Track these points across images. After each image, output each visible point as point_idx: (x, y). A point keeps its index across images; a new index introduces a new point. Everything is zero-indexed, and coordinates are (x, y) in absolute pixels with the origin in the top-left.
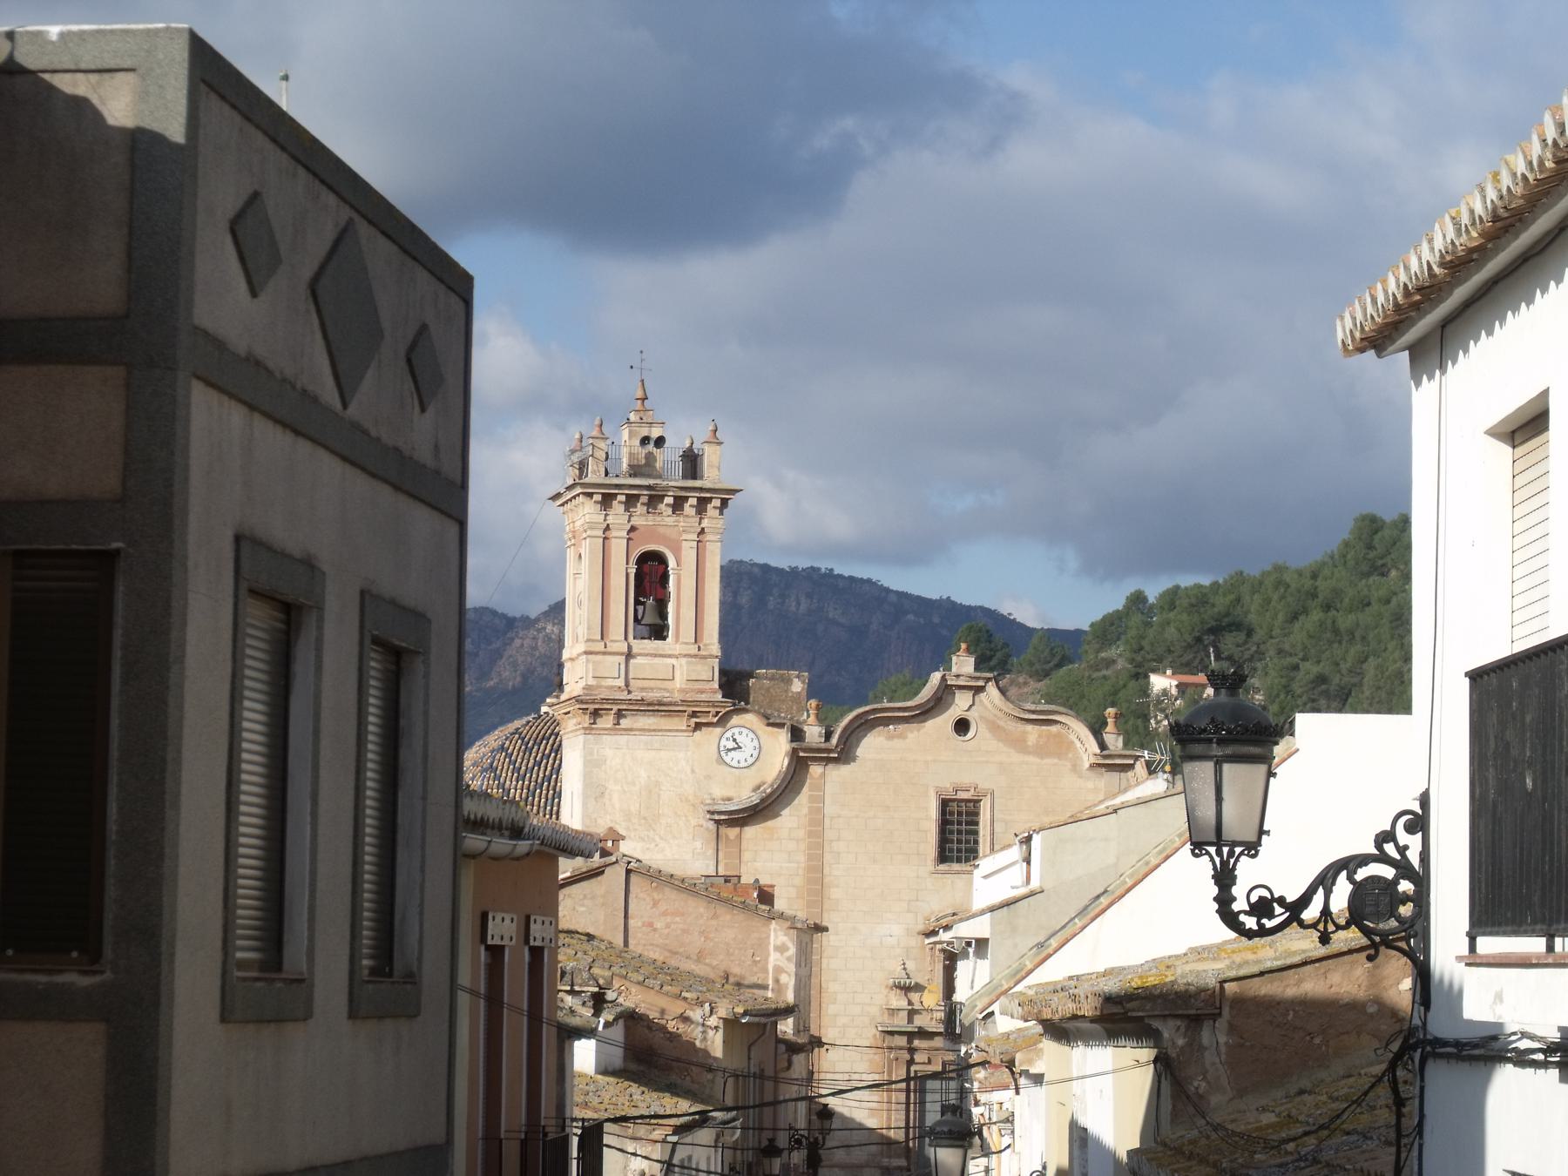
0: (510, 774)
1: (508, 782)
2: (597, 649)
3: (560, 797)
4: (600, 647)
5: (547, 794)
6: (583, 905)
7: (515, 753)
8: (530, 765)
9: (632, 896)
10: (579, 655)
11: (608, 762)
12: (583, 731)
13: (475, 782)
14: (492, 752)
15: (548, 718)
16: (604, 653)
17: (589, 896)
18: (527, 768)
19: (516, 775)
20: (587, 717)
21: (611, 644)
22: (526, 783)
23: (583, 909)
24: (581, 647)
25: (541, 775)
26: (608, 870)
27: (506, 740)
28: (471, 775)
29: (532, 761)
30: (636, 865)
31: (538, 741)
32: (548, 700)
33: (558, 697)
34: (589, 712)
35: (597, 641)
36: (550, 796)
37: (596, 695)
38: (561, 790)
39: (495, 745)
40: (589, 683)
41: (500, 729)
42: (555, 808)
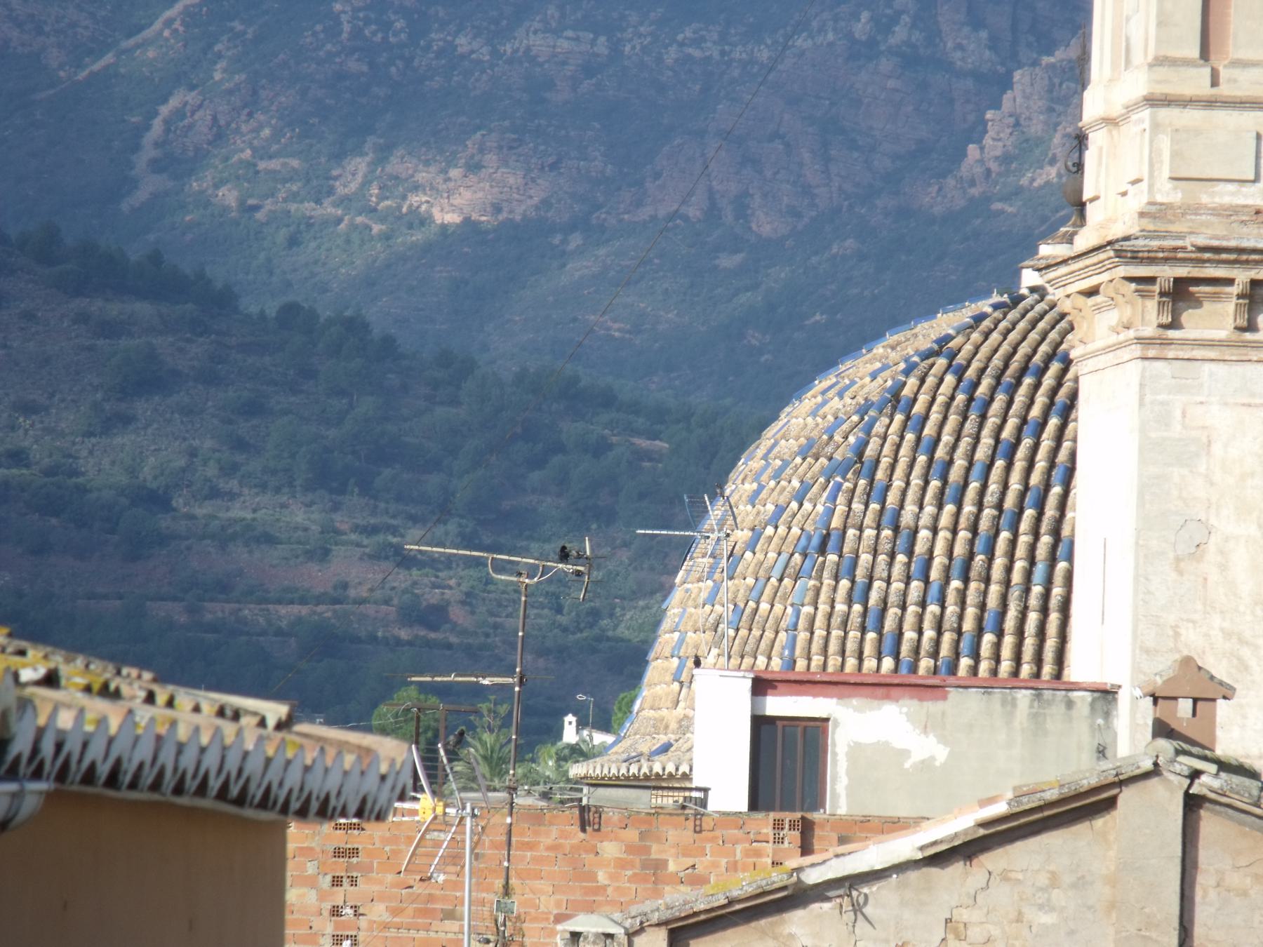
0: (916, 481)
1: (910, 508)
2: (1188, 90)
3: (1070, 558)
4: (1196, 82)
5: (1032, 548)
6: (1046, 907)
7: (935, 417)
8: (981, 453)
9: (1204, 881)
10: (1130, 108)
11: (1217, 449)
12: (1137, 350)
13: (807, 506)
14: (862, 411)
15: (1039, 308)
16: (1210, 103)
17: (1067, 879)
18: (971, 463)
19: (935, 484)
20: (1152, 305)
21: (1236, 73)
22: (968, 508)
23: (1047, 919)
24: (1137, 84)
25: (1015, 485)
26: (1127, 797)
27: (907, 372)
28: (796, 483)
29: (986, 441)
30: (1216, 784)
31: (1008, 378)
32: (1046, 250)
33: (1069, 239)
34: (1157, 288)
35: (1186, 63)
36: (1042, 551)
37: (1181, 236)
38: (1073, 535)
39: (873, 389)
40: (1159, 198)
41: (891, 339)
42: (1057, 591)
